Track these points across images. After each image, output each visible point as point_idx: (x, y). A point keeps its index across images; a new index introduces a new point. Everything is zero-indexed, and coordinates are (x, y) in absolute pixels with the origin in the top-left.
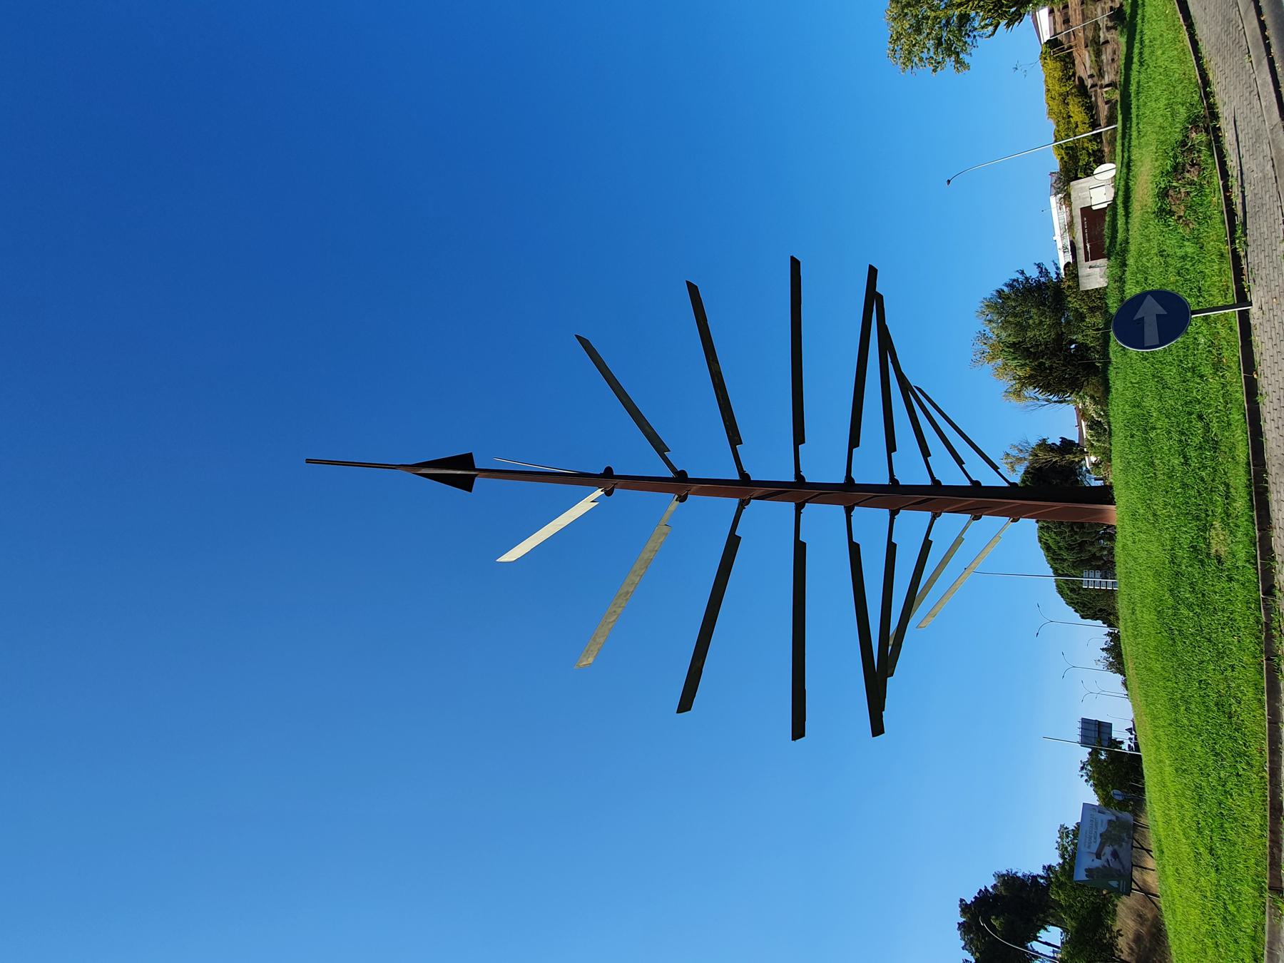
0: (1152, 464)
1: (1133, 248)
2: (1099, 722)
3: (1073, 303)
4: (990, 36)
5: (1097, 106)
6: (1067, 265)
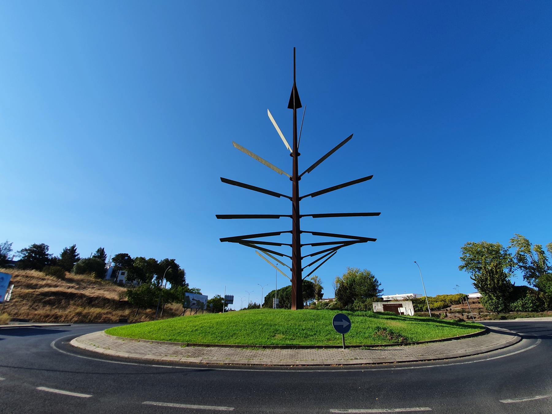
0: (304, 321)
1: (375, 320)
2: (233, 301)
3: (368, 300)
4: (471, 278)
6: (382, 299)
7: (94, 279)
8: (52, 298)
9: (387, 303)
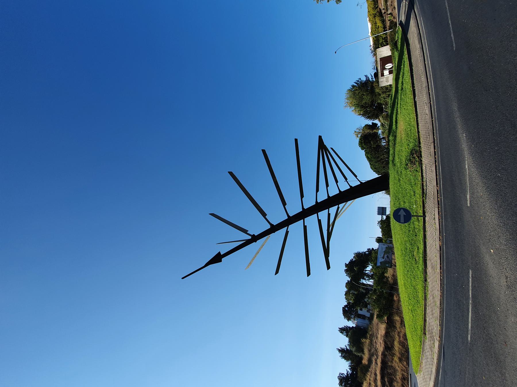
3: (377, 91)
5: (386, 21)
7: (368, 340)
8: (386, 379)
9: (379, 72)
